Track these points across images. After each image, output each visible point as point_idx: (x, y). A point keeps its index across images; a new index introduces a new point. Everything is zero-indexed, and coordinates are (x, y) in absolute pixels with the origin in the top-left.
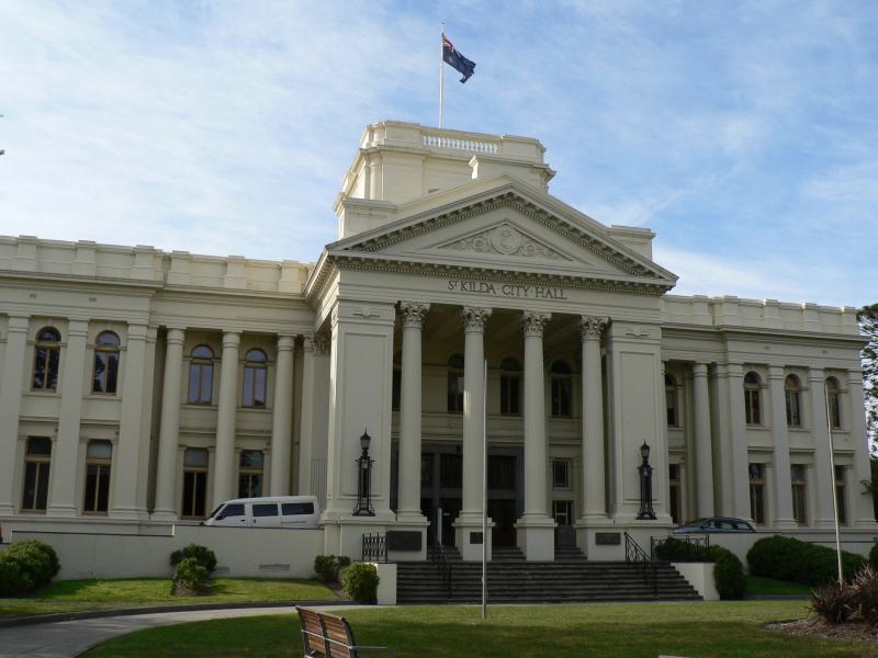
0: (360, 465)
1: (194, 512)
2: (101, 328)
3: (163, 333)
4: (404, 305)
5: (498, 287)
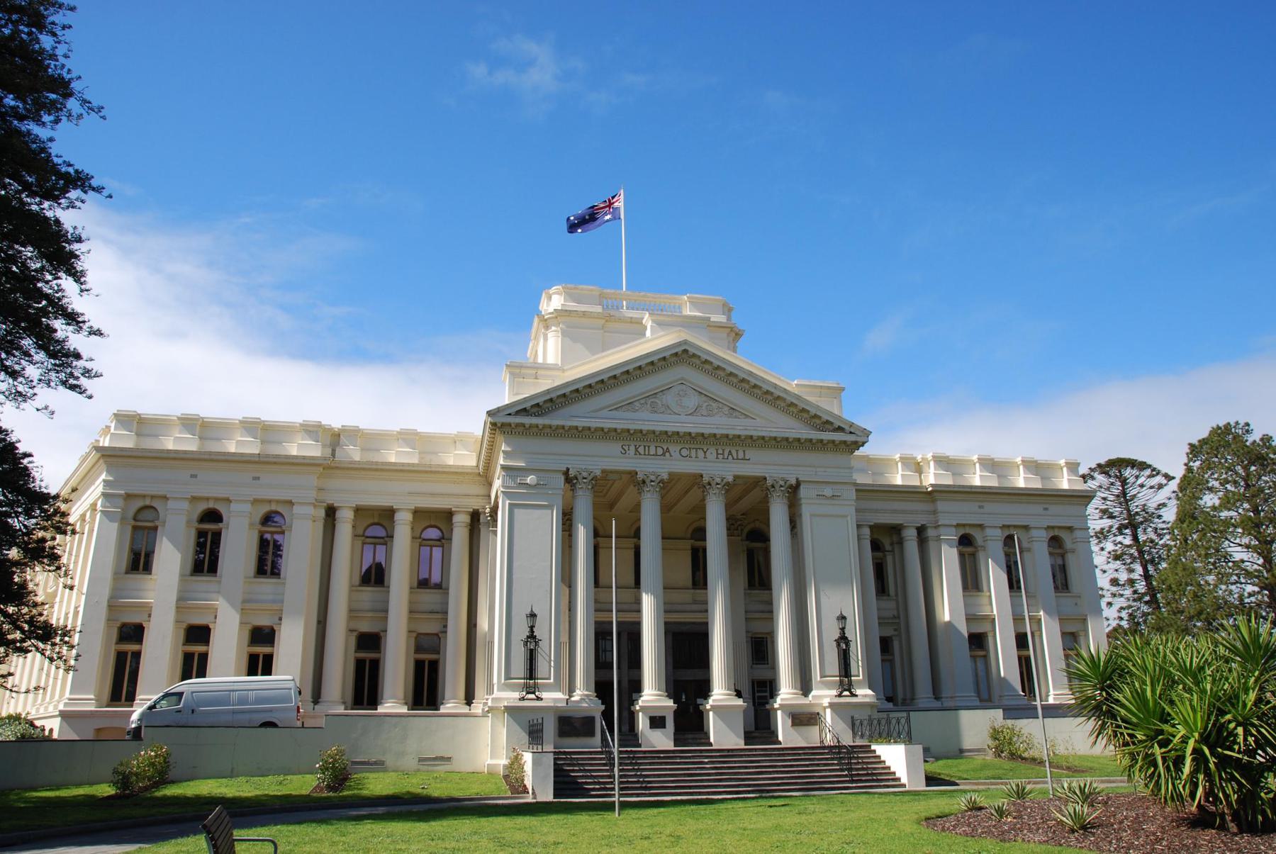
0: (838, 645)
2: (140, 503)
3: (331, 512)
4: (572, 473)
5: (674, 449)
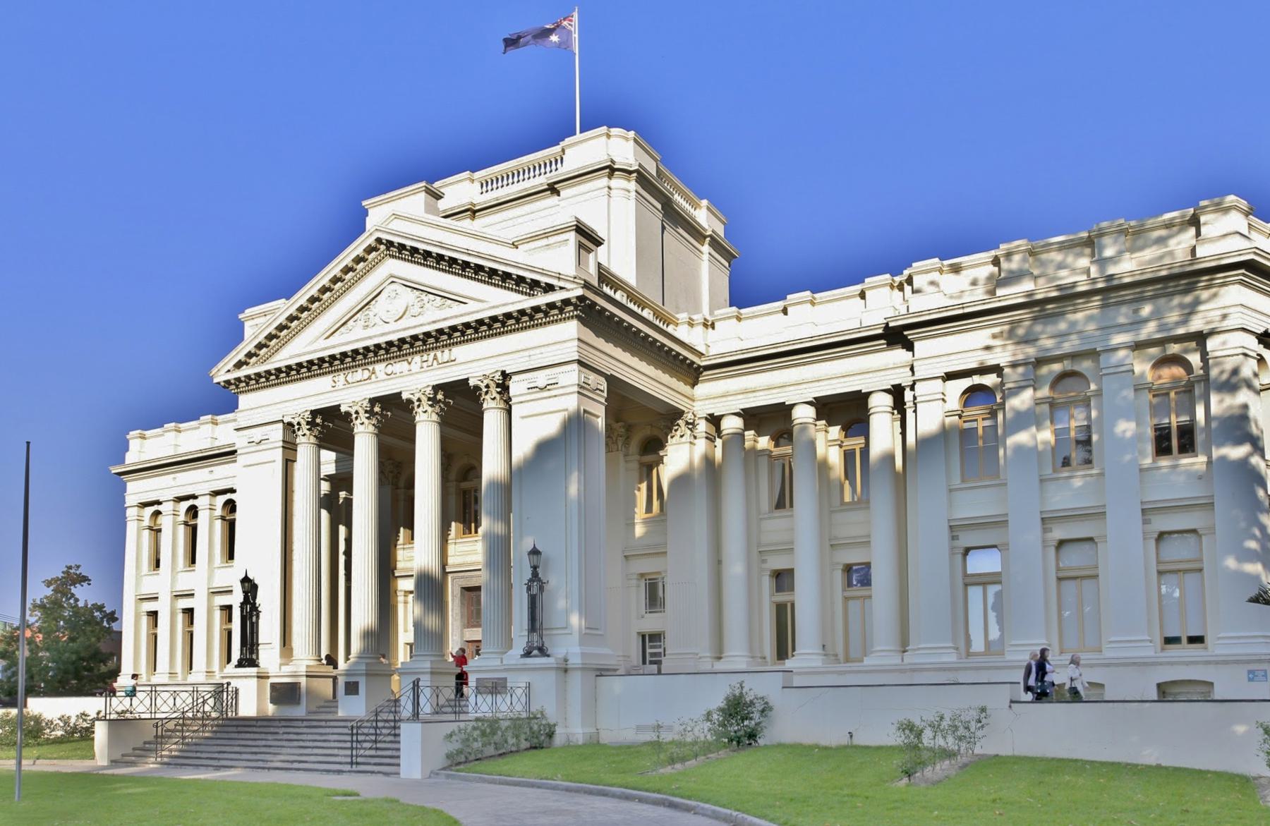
0: (529, 589)
1: (590, 650)
2: (966, 383)
